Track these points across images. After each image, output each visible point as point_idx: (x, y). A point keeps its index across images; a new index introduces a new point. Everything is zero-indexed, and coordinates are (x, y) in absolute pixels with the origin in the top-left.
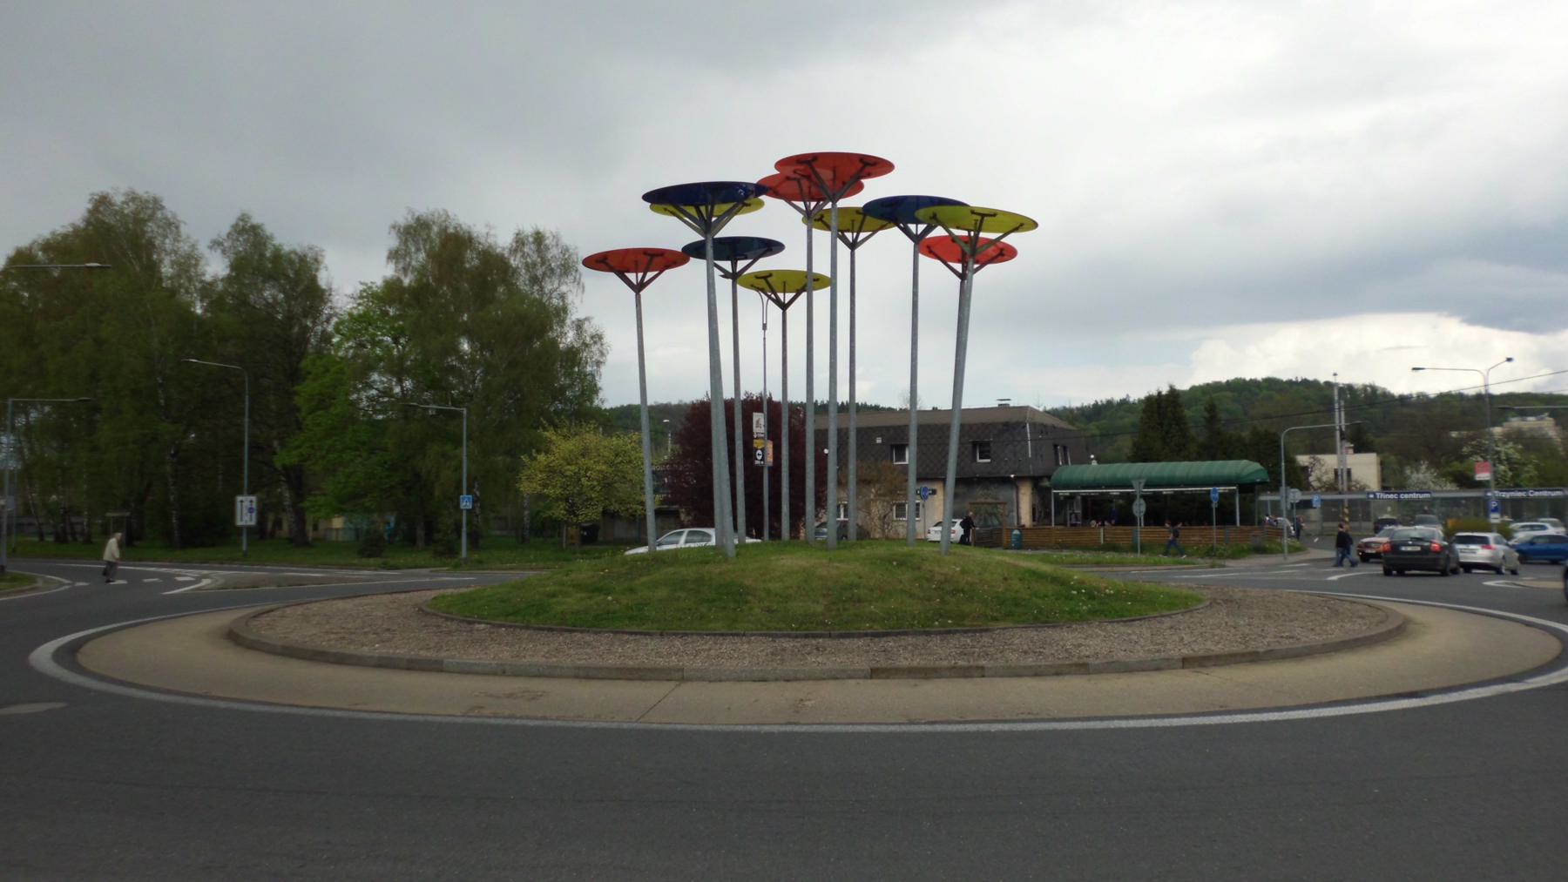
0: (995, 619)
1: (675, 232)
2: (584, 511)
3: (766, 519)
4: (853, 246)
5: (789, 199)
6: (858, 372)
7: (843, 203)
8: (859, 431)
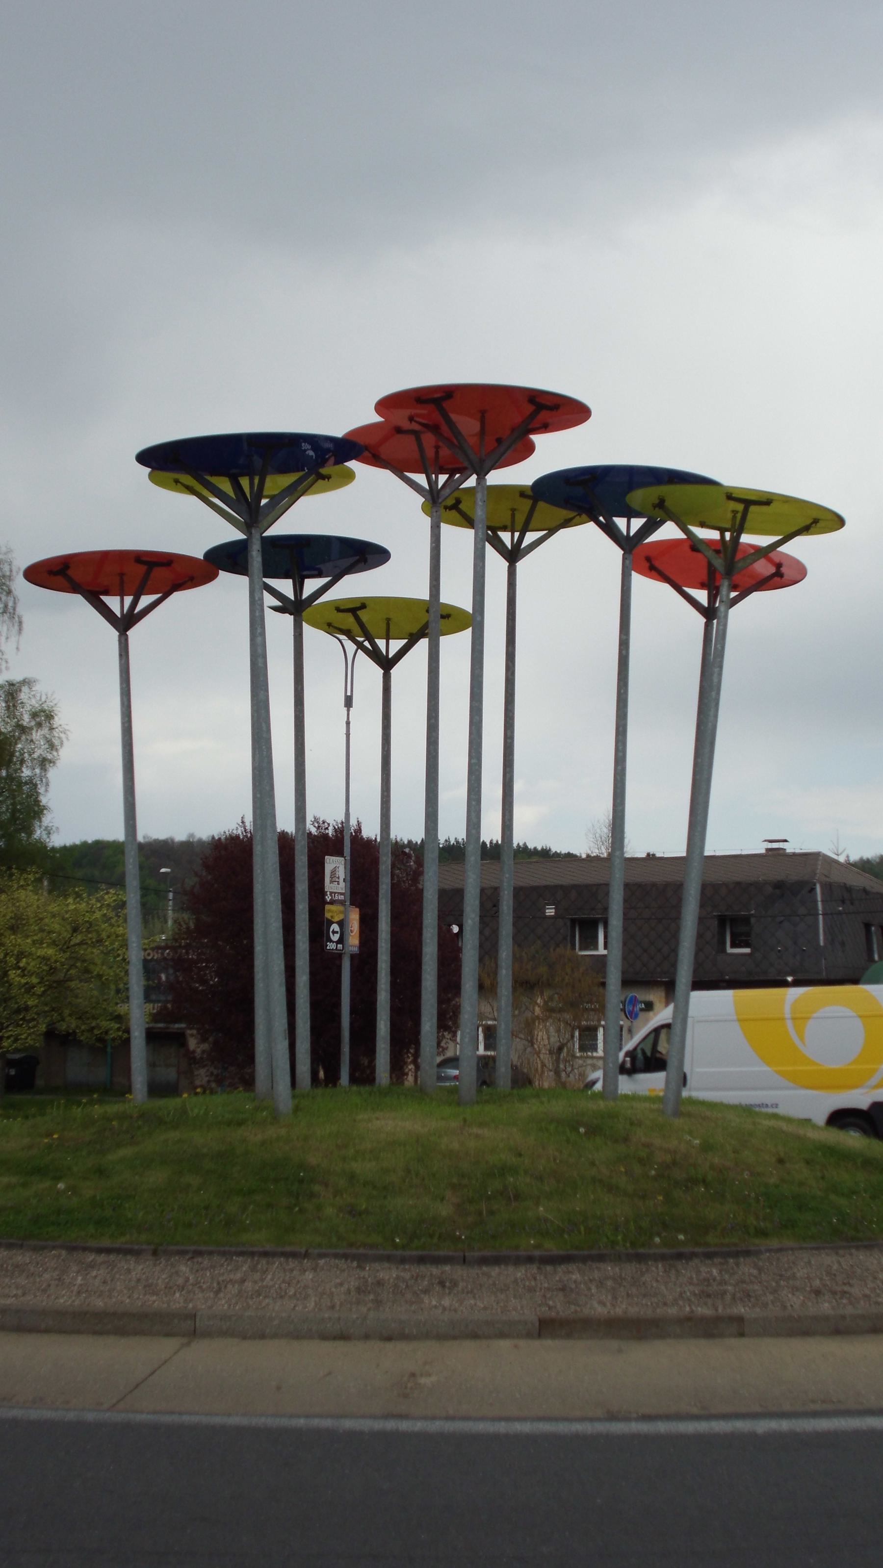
0: (763, 1233)
1: (193, 524)
2: (12, 1031)
3: (346, 1049)
4: (513, 555)
5: (399, 469)
6: (518, 786)
7: (497, 477)
8: (518, 892)
